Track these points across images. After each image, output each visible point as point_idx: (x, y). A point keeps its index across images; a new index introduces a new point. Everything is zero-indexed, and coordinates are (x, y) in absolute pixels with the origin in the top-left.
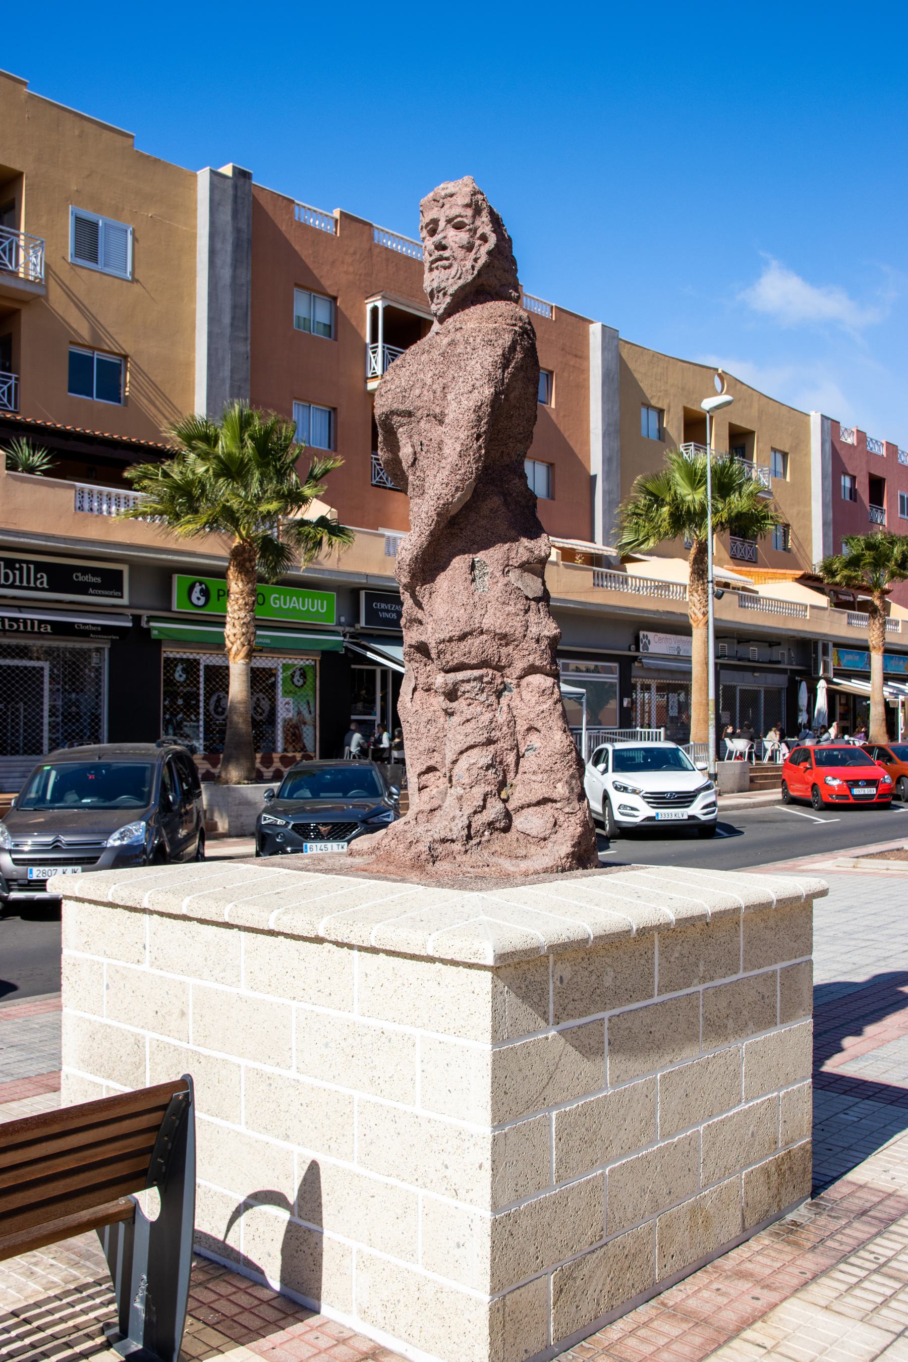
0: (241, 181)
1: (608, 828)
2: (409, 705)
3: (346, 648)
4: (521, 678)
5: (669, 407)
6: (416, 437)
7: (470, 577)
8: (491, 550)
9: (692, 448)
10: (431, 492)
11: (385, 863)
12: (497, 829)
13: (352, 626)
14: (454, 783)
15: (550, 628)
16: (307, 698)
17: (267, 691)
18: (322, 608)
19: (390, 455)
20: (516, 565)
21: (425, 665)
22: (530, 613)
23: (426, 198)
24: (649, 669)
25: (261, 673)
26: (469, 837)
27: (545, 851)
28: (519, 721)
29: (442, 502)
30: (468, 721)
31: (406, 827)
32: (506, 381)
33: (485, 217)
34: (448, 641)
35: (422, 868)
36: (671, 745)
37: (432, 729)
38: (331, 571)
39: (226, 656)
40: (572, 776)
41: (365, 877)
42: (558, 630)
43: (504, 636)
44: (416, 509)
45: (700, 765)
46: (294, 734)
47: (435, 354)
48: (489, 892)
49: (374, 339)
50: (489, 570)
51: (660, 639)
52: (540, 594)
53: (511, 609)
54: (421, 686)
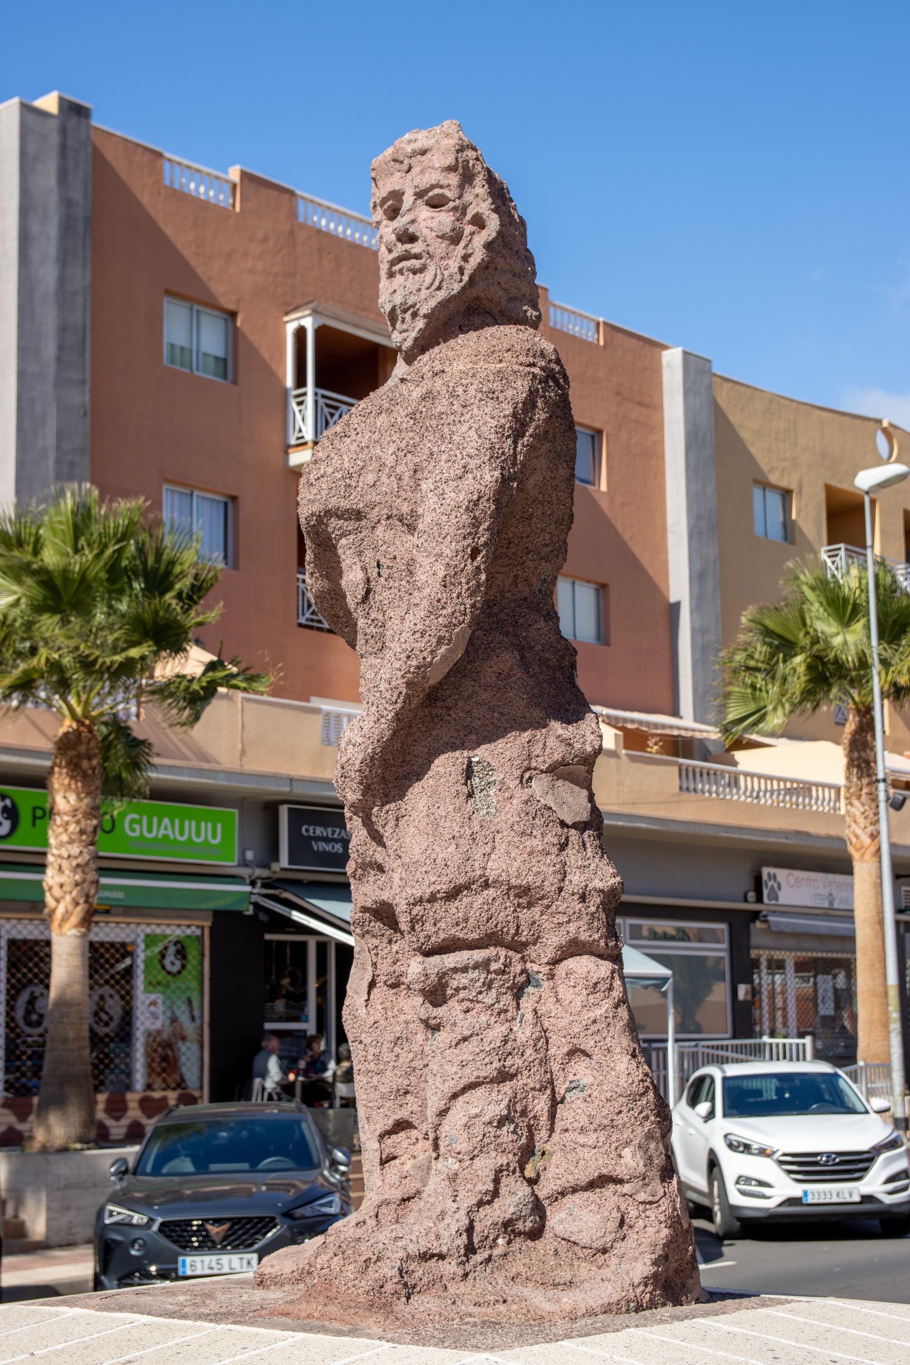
0: (73, 122)
1: (718, 1218)
2: (362, 1012)
3: (256, 906)
4: (555, 962)
5: (800, 485)
6: (369, 554)
7: (465, 790)
8: (500, 744)
9: (842, 553)
10: (396, 647)
11: (321, 1299)
12: (520, 1234)
13: (266, 866)
14: (442, 1149)
15: (603, 876)
16: (189, 993)
17: (117, 982)
18: (214, 836)
19: (326, 584)
20: (544, 768)
21: (390, 942)
22: (569, 850)
23: (380, 157)
24: (781, 934)
25: (107, 950)
26: (470, 1249)
27: (606, 1272)
28: (553, 1039)
29: (414, 663)
30: (465, 1039)
31: (359, 1232)
32: (520, 458)
33: (480, 188)
34: (429, 901)
35: (386, 1308)
36: (824, 1068)
37: (403, 1055)
38: (229, 774)
39: (46, 922)
40: (649, 1136)
41: (285, 1328)
42: (618, 879)
43: (525, 891)
44: (370, 675)
45: (878, 1103)
46: (164, 1060)
47: (400, 414)
48: (507, 1352)
49: (301, 381)
50: (498, 776)
51: (798, 881)
52: (585, 816)
53: (536, 843)
54: (384, 978)
